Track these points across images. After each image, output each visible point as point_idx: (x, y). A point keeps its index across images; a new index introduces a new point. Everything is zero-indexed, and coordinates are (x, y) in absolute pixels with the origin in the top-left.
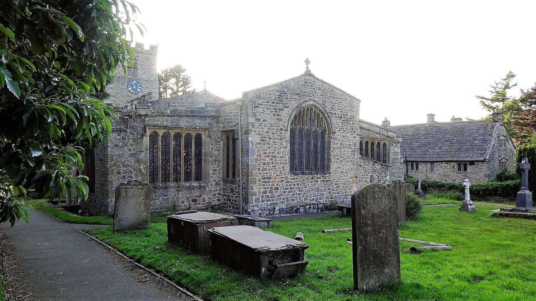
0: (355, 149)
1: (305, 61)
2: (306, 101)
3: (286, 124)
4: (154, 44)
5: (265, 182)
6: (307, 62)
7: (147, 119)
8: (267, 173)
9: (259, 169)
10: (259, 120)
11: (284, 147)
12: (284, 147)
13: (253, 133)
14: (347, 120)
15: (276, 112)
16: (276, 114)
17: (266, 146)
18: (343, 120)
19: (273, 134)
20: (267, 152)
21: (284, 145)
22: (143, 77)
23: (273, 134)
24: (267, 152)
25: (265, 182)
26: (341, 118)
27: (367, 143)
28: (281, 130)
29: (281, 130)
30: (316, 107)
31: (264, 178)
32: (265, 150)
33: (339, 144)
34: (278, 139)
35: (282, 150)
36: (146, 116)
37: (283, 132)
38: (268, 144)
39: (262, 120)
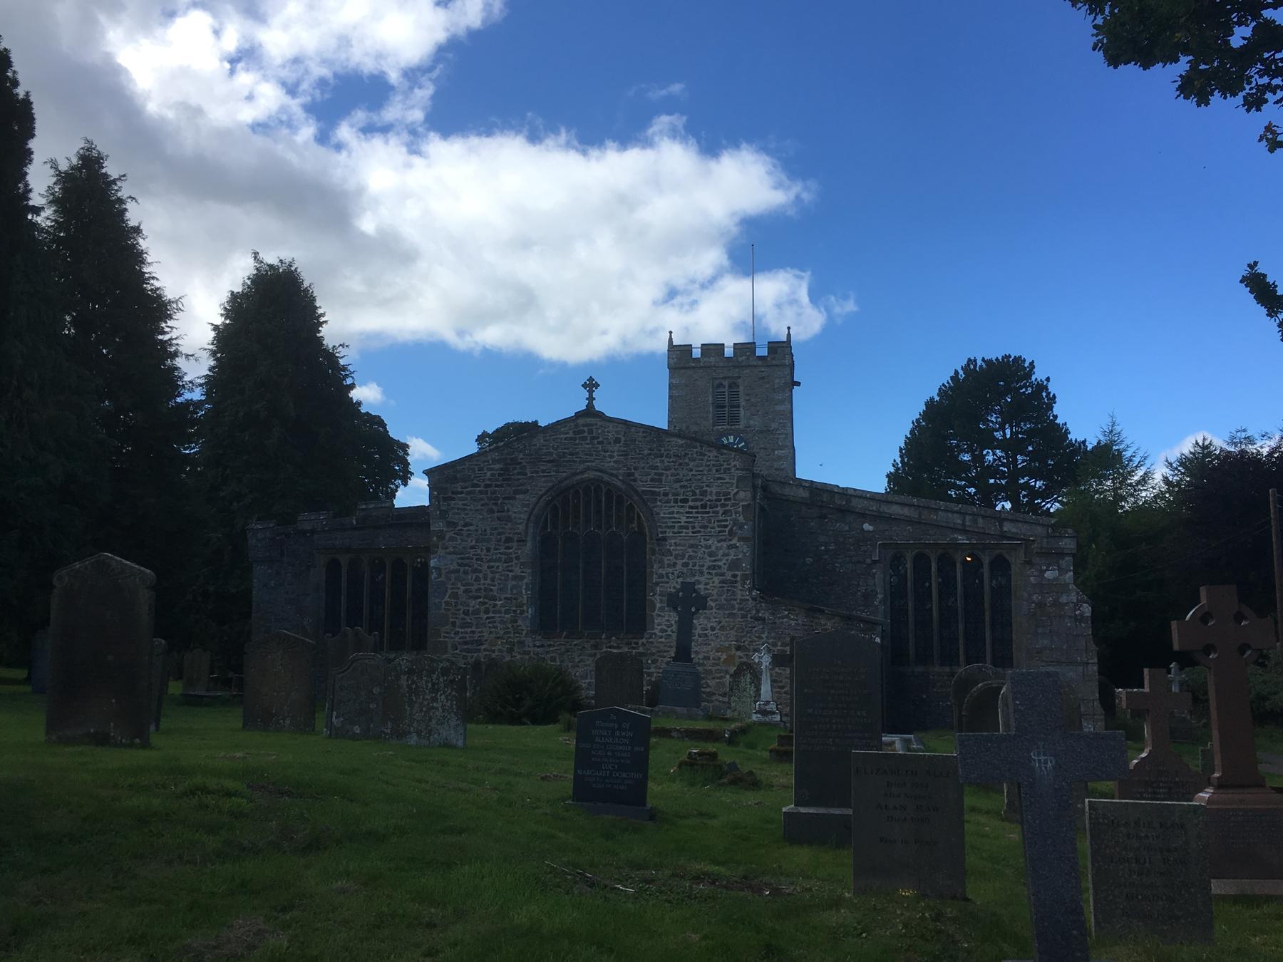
0: (735, 576)
1: (585, 386)
2: (575, 474)
3: (521, 528)
4: (585, 380)
5: (468, 651)
6: (591, 385)
7: (316, 537)
8: (473, 632)
9: (454, 624)
10: (454, 525)
11: (515, 578)
12: (515, 578)
13: (441, 552)
14: (704, 506)
15: (496, 504)
16: (495, 508)
17: (471, 577)
18: (691, 507)
19: (488, 550)
20: (473, 588)
21: (517, 571)
22: (752, 422)
23: (488, 550)
24: (473, 588)
25: (468, 651)
26: (686, 501)
27: (921, 562)
28: (508, 540)
29: (508, 540)
30: (607, 483)
31: (466, 643)
32: (468, 584)
33: (679, 567)
34: (499, 560)
35: (511, 583)
36: (313, 531)
37: (515, 545)
38: (475, 571)
39: (462, 523)
